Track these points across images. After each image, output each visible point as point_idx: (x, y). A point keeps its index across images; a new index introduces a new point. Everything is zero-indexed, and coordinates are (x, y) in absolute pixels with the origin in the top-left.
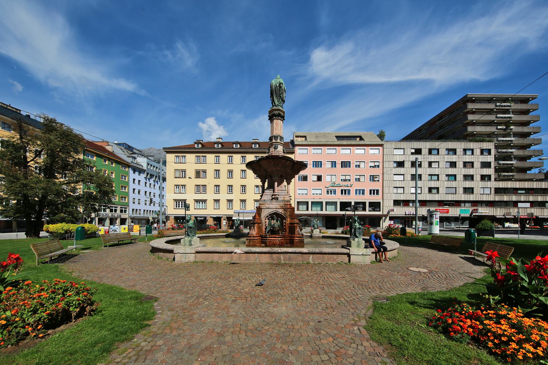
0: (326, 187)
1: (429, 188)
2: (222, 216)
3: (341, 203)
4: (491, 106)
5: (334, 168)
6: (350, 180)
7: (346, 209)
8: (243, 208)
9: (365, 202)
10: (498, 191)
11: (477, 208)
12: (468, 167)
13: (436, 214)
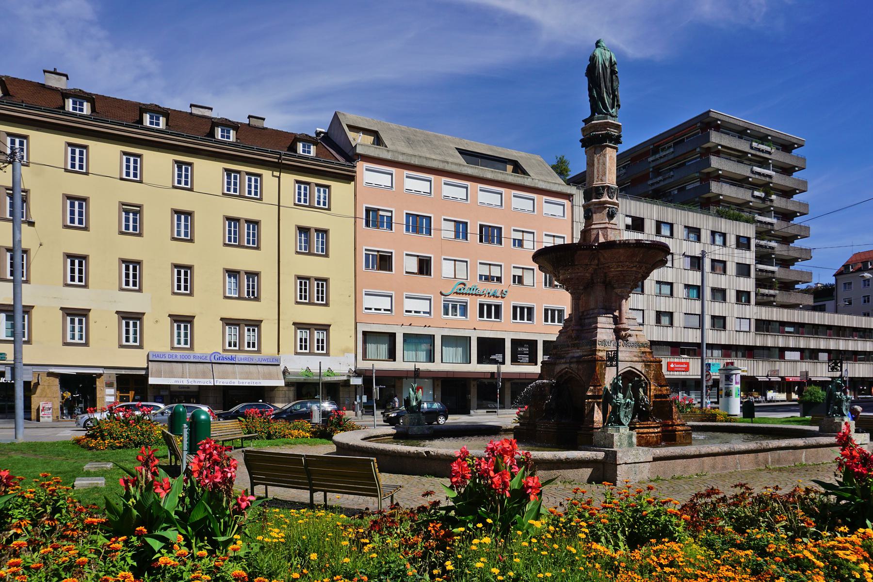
0: (441, 294)
1: (657, 311)
2: (100, 371)
3: (480, 340)
4: (743, 146)
5: (460, 240)
6: (499, 279)
7: (493, 357)
8: (182, 345)
9: (536, 341)
10: (763, 326)
11: (730, 361)
12: (718, 272)
13: (736, 374)
